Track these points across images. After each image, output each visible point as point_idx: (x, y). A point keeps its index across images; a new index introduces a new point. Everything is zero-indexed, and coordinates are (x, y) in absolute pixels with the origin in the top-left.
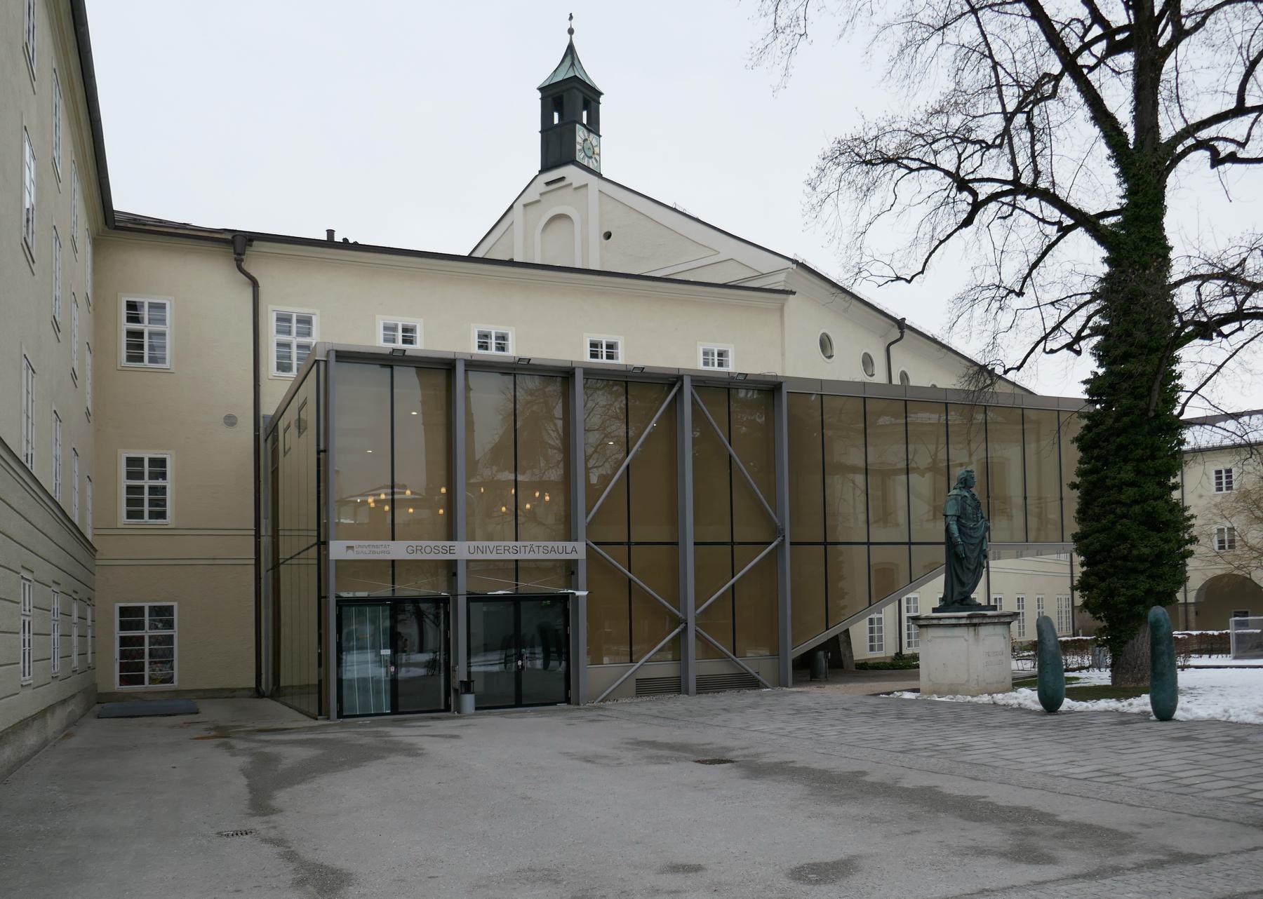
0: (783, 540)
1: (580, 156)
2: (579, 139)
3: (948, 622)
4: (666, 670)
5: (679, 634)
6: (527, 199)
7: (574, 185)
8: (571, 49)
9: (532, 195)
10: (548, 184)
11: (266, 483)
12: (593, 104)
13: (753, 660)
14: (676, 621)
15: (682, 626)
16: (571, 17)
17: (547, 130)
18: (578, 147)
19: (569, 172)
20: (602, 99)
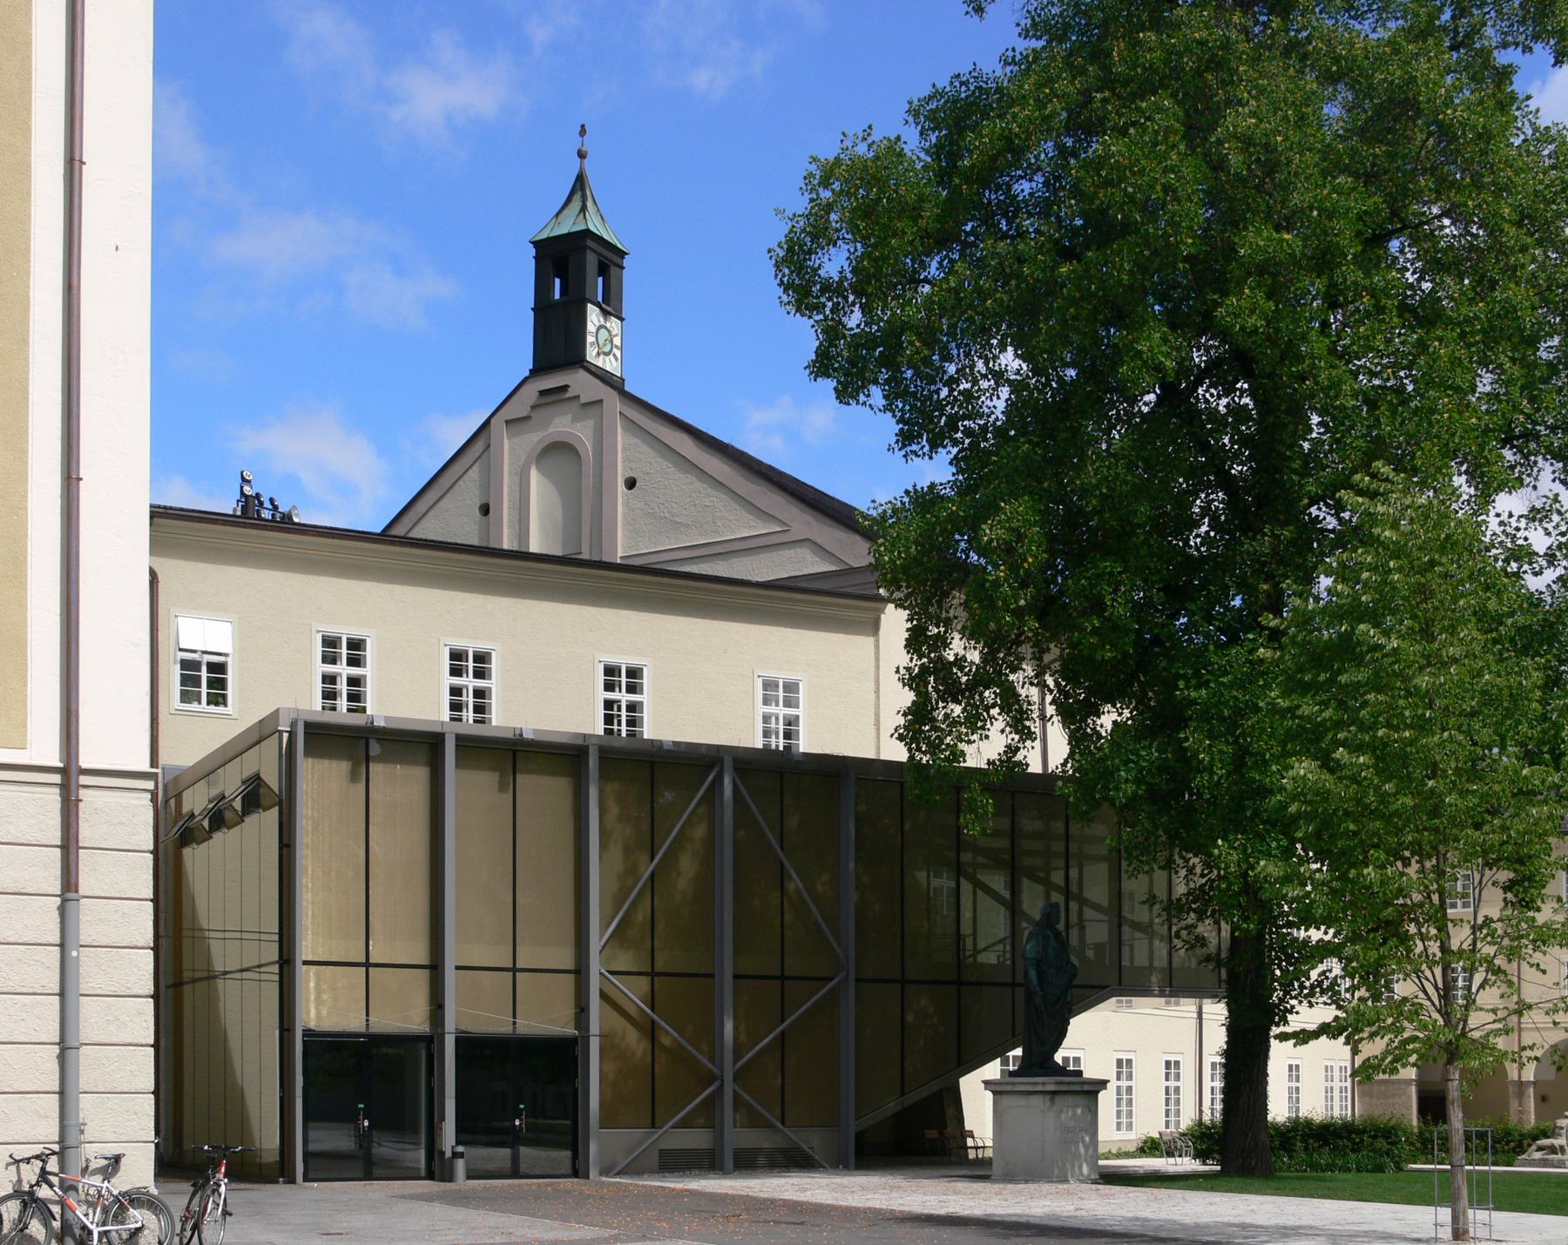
0: (847, 977)
1: (591, 355)
2: (591, 328)
3: (1022, 1088)
4: (695, 1139)
5: (713, 1093)
6: (512, 411)
7: (583, 400)
8: (580, 182)
9: (517, 409)
10: (543, 393)
11: (166, 862)
12: (613, 271)
13: (812, 1141)
14: (711, 1078)
15: (717, 1083)
16: (583, 131)
17: (542, 307)
18: (590, 339)
19: (577, 381)
20: (626, 262)
